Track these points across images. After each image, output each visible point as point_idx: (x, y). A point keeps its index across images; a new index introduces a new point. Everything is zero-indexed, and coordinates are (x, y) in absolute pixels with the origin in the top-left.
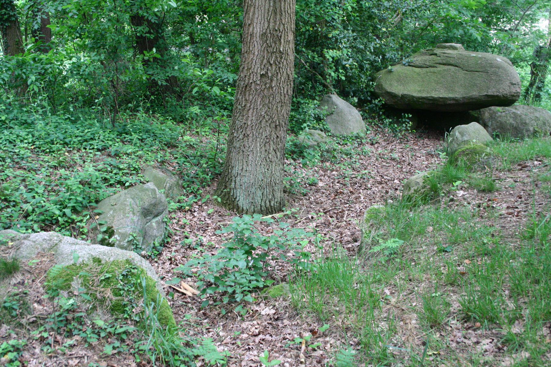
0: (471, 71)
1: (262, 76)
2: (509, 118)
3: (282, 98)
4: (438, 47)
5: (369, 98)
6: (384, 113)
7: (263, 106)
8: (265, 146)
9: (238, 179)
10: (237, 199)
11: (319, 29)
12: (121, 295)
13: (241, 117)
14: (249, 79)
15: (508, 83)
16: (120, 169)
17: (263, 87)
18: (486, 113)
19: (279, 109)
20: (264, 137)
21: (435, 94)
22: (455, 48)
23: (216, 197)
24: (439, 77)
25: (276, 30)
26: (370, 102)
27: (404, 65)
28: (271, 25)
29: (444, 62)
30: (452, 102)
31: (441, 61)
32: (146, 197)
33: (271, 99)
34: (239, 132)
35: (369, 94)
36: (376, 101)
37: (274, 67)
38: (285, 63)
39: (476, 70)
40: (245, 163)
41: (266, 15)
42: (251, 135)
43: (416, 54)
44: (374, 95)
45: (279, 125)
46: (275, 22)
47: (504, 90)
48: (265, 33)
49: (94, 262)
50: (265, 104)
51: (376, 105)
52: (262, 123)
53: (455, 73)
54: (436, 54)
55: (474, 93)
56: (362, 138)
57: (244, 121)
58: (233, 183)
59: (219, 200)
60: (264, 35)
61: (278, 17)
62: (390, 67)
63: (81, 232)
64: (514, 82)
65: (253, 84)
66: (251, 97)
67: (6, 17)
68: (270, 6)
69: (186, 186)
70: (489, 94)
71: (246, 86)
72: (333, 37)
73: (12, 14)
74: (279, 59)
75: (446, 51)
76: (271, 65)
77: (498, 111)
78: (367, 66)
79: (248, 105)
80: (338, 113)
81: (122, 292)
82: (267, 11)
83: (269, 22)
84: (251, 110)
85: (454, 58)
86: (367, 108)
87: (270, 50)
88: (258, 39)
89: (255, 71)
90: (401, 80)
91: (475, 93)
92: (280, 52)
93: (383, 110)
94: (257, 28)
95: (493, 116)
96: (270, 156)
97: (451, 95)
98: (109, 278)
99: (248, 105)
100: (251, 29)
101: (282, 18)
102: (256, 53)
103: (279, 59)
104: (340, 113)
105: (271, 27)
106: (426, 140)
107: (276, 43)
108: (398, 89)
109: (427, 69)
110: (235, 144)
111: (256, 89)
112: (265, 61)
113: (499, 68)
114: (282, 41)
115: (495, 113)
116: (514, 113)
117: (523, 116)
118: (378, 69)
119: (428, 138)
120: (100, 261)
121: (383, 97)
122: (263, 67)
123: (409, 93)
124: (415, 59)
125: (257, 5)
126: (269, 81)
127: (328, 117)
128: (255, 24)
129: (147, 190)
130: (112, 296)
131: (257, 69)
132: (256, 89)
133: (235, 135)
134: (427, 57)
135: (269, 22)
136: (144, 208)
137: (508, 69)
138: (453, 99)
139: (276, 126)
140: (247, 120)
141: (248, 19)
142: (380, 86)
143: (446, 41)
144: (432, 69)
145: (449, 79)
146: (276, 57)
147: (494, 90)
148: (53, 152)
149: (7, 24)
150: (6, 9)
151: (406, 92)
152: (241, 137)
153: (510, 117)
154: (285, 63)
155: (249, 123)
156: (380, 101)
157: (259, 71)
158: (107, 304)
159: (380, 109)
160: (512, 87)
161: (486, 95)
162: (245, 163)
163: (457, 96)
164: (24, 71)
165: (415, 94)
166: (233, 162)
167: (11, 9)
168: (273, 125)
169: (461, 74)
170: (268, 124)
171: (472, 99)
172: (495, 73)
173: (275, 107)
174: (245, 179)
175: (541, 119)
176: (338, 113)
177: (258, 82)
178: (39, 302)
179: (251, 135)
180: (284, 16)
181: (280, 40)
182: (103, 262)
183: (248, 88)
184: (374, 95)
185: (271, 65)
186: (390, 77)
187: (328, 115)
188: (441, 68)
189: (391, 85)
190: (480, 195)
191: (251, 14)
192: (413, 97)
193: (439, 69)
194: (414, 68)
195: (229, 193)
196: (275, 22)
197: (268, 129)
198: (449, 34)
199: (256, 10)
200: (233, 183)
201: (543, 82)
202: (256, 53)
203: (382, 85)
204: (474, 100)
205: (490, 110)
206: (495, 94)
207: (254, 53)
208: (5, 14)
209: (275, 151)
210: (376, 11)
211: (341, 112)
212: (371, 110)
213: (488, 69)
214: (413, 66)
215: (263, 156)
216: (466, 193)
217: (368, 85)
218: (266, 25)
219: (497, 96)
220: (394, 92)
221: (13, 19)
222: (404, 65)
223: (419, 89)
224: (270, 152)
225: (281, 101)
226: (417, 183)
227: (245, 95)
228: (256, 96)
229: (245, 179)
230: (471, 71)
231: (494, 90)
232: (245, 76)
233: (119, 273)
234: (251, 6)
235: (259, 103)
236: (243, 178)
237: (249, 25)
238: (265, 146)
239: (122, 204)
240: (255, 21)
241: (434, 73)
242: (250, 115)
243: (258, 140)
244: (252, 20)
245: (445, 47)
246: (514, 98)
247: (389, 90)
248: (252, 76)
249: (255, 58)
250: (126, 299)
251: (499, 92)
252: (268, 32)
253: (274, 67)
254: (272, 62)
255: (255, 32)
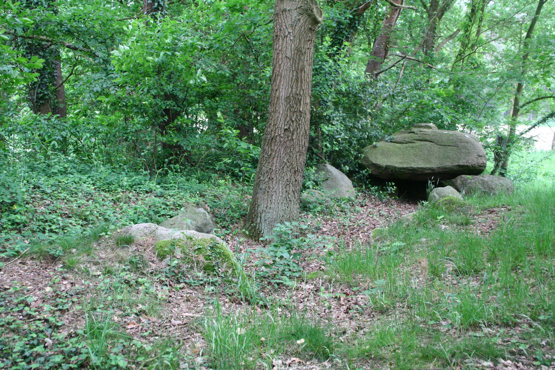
0: (444, 146)
1: (285, 130)
2: (477, 184)
3: (301, 148)
4: (415, 127)
5: (357, 170)
6: (370, 183)
7: (286, 155)
8: (286, 187)
9: (263, 215)
10: (262, 232)
11: (315, 110)
12: (210, 260)
13: (267, 164)
14: (275, 133)
15: (475, 155)
16: (167, 205)
17: (286, 139)
18: (459, 180)
19: (298, 158)
20: (285, 180)
21: (414, 165)
22: (430, 127)
23: (244, 230)
24: (417, 150)
25: (297, 94)
26: (359, 172)
27: (387, 141)
28: (294, 90)
29: (421, 138)
30: (429, 171)
31: (418, 138)
32: (198, 219)
33: (292, 149)
34: (265, 176)
35: (357, 165)
36: (364, 172)
37: (295, 123)
38: (303, 121)
39: (448, 144)
40: (269, 202)
41: (290, 82)
42: (275, 178)
43: (396, 133)
44: (362, 167)
45: (297, 171)
46: (297, 88)
47: (471, 161)
48: (289, 97)
49: (187, 239)
50: (287, 153)
51: (364, 175)
52: (284, 169)
53: (430, 147)
54: (414, 132)
55: (448, 164)
56: (352, 201)
57: (270, 167)
58: (259, 219)
59: (247, 233)
60: (288, 98)
61: (299, 84)
62: (374, 143)
63: (367, 51)
64: (481, 155)
65: (278, 137)
66: (276, 147)
67: (41, 95)
68: (293, 76)
69: (219, 222)
70: (460, 164)
71: (272, 139)
72: (327, 115)
73: (46, 93)
74: (299, 117)
75: (422, 129)
76: (293, 121)
77: (468, 178)
78: (355, 142)
79: (274, 154)
80: (332, 179)
81: (211, 257)
82: (290, 79)
83: (292, 88)
84: (276, 158)
85: (429, 135)
86: (356, 177)
87: (292, 109)
88: (283, 101)
89: (280, 126)
90: (384, 153)
91: (448, 164)
92: (300, 111)
93: (369, 180)
94: (283, 93)
95: (464, 184)
96: (290, 196)
97: (428, 166)
98: (200, 248)
99: (274, 154)
100: (278, 93)
101: (303, 85)
102: (281, 112)
103: (299, 117)
104: (334, 179)
105: (293, 92)
106: (407, 205)
107: (297, 105)
108: (383, 161)
109: (407, 145)
110: (261, 186)
111: (280, 141)
112: (288, 118)
113: (468, 143)
114: (302, 103)
115: (466, 180)
116: (482, 180)
117: (490, 183)
118: (363, 146)
119: (409, 204)
120: (191, 239)
121: (369, 169)
122: (286, 123)
123: (391, 164)
124: (396, 137)
125: (283, 75)
126: (290, 135)
127: (324, 182)
128: (281, 90)
129: (199, 213)
130: (204, 260)
131: (282, 124)
132: (280, 141)
133: (261, 178)
134: (406, 135)
135: (292, 88)
136: (198, 227)
137: (475, 143)
138: (430, 169)
139: (295, 171)
140: (272, 166)
141: (275, 86)
142: (366, 158)
143: (421, 122)
144: (411, 145)
145: (426, 152)
146: (297, 116)
147: (464, 161)
148: (111, 191)
149: (41, 102)
150: (42, 89)
151: (389, 164)
152: (267, 180)
153: (479, 183)
154: (303, 121)
155: (274, 168)
156: (368, 171)
157: (283, 127)
158: (201, 265)
159: (367, 178)
160: (479, 158)
161: (458, 165)
162: (269, 202)
163: (433, 166)
164: (78, 130)
165: (397, 165)
166: (259, 201)
167: (46, 89)
168: (293, 171)
169: (435, 148)
170: (289, 170)
171: (446, 168)
172: (465, 148)
173: (295, 156)
174: (269, 215)
175: (505, 185)
176: (332, 179)
177: (282, 135)
178: (153, 262)
179: (275, 178)
180: (303, 84)
181: (300, 102)
182: (194, 239)
183: (274, 140)
184: (362, 167)
185: (293, 121)
186: (375, 151)
187: (324, 181)
188: (418, 143)
189: (376, 158)
190: (459, 227)
191: (278, 82)
192: (395, 168)
193: (417, 144)
194: (395, 144)
195: (255, 227)
196: (297, 88)
197: (289, 173)
198: (423, 118)
199: (282, 78)
200: (259, 219)
201: (506, 169)
202: (281, 112)
203: (368, 158)
204: (448, 170)
205: (461, 178)
206: (466, 164)
207: (279, 113)
208: (41, 93)
209: (294, 192)
210: (362, 96)
211: (335, 178)
212: (360, 178)
213: (459, 143)
214: (394, 142)
215: (284, 196)
216: (447, 226)
217: (356, 158)
218: (290, 90)
219: (467, 166)
220: (379, 163)
221: (47, 97)
222: (387, 141)
223: (400, 161)
224: (290, 192)
225: (299, 151)
226: (408, 220)
227: (271, 146)
228: (280, 147)
229: (269, 215)
230: (444, 146)
231: (464, 161)
232: (272, 131)
233: (207, 246)
234: (278, 75)
235: (282, 152)
236: (268, 214)
237: (276, 90)
238: (286, 187)
239: (179, 223)
240: (281, 87)
241: (413, 147)
242: (275, 162)
243: (281, 182)
244: (279, 86)
245: (422, 127)
246: (481, 168)
247: (374, 162)
248: (277, 130)
249: (280, 116)
250: (214, 263)
251: (469, 163)
252: (291, 95)
253: (295, 123)
254: (293, 119)
255: (281, 96)
